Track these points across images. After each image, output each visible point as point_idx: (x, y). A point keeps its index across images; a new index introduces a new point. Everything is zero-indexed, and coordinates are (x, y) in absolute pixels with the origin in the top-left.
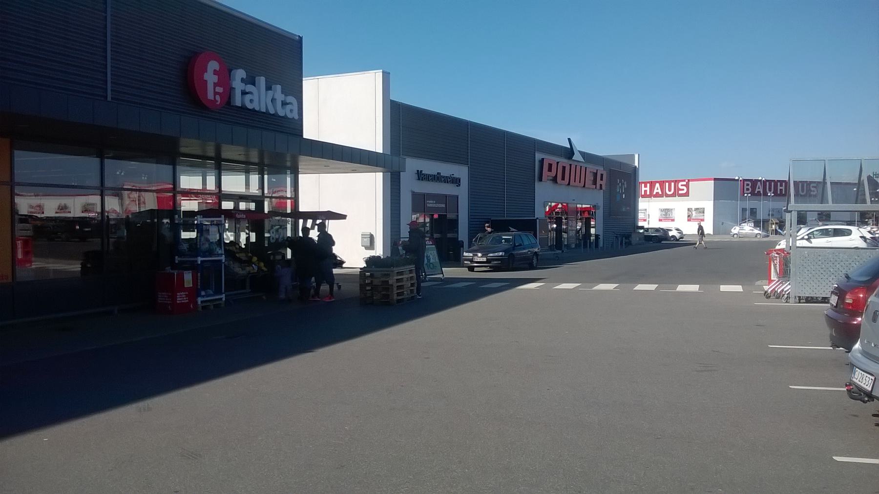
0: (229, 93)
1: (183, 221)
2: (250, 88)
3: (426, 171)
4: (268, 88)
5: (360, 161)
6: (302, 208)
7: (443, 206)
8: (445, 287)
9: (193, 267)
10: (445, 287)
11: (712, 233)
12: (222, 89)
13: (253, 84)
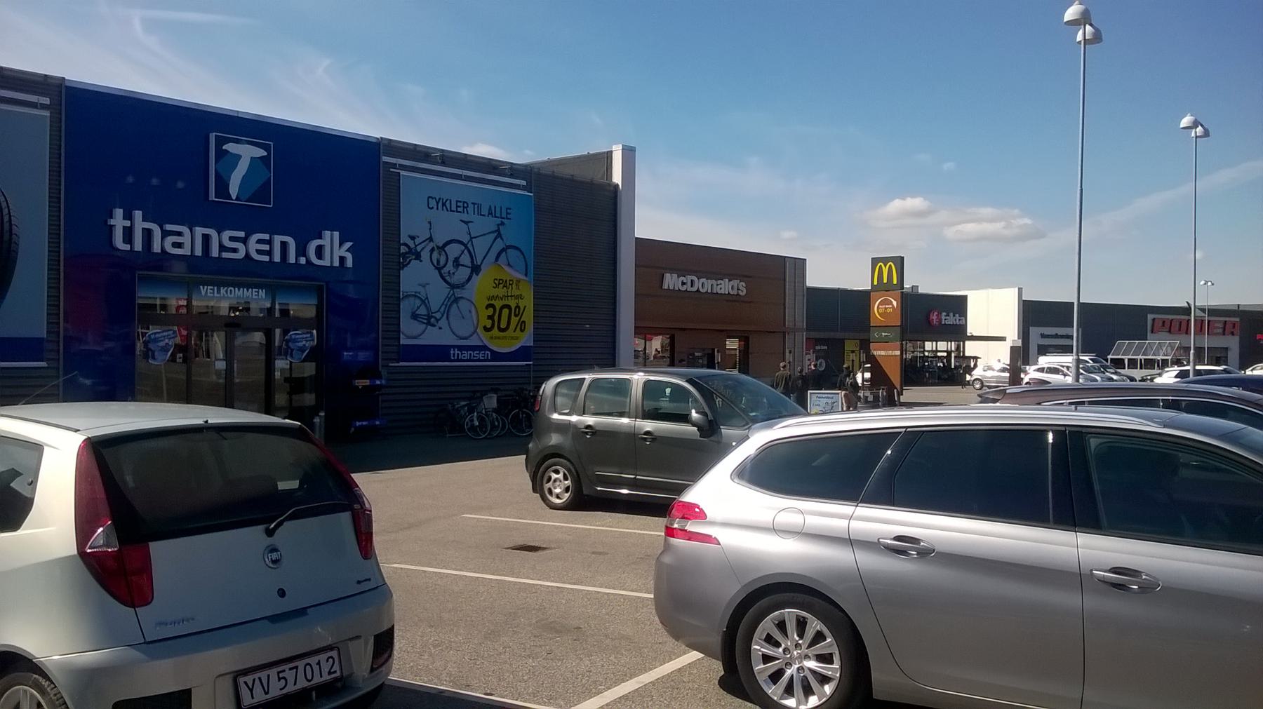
0: (941, 320)
1: (1085, 351)
2: (947, 317)
3: (1046, 333)
4: (954, 316)
5: (538, 317)
6: (967, 354)
7: (826, 348)
8: (93, 550)
9: (930, 372)
10: (93, 550)
11: (525, 456)
12: (279, 261)
13: (949, 316)
